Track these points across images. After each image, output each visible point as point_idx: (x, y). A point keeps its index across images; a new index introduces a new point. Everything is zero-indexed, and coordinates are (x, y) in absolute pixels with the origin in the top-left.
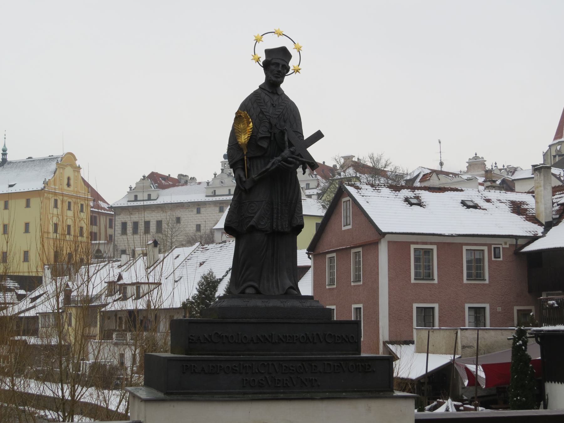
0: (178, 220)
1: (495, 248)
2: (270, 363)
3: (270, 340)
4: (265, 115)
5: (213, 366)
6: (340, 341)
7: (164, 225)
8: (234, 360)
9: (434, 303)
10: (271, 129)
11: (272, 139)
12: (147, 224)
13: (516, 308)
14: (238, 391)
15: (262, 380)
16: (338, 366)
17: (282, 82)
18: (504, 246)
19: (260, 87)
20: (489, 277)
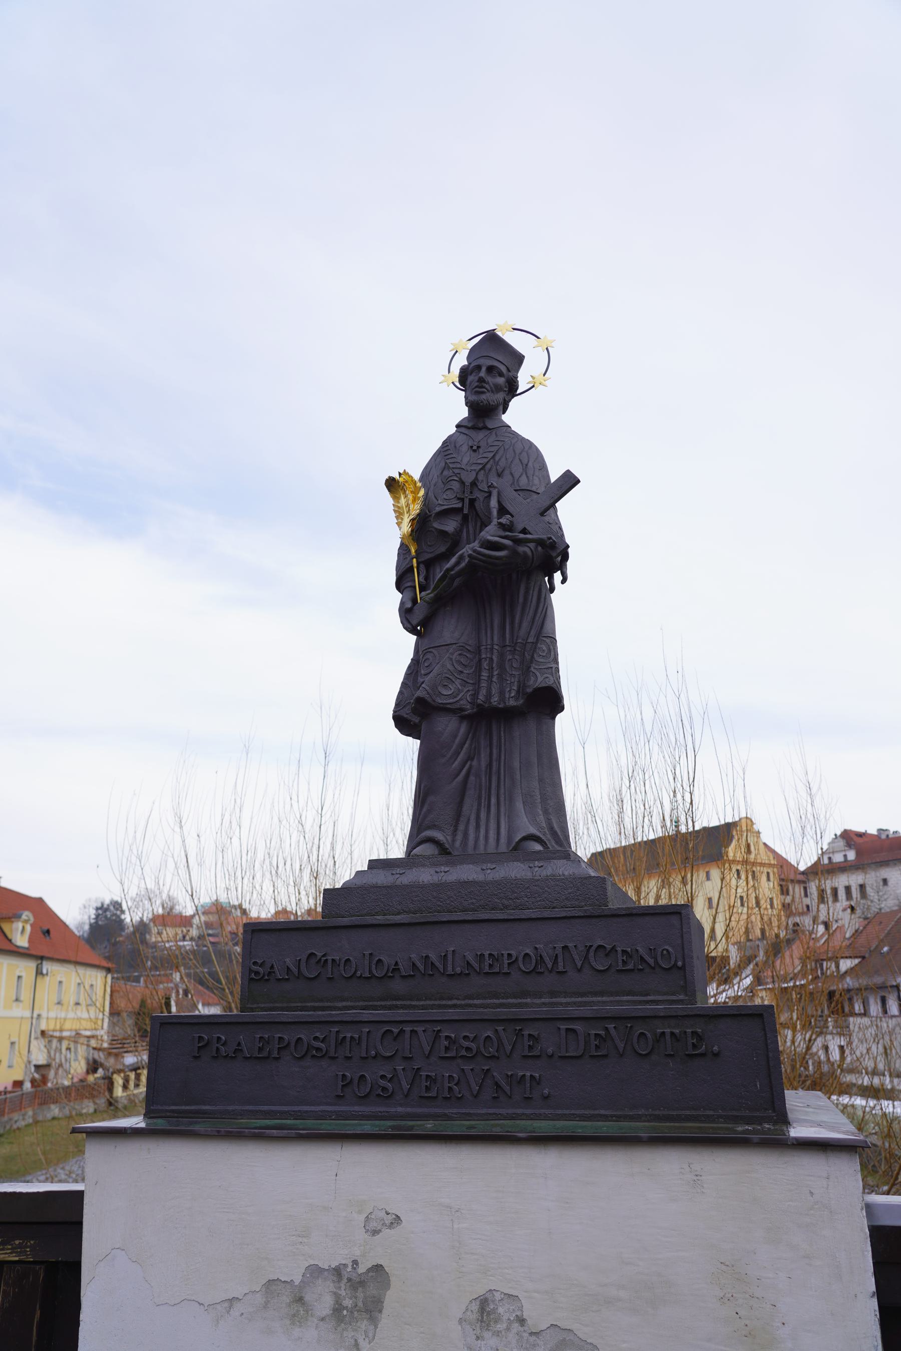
0: (885, 882)
6: (630, 967)
7: (868, 889)
8: (227, 1023)
12: (848, 889)
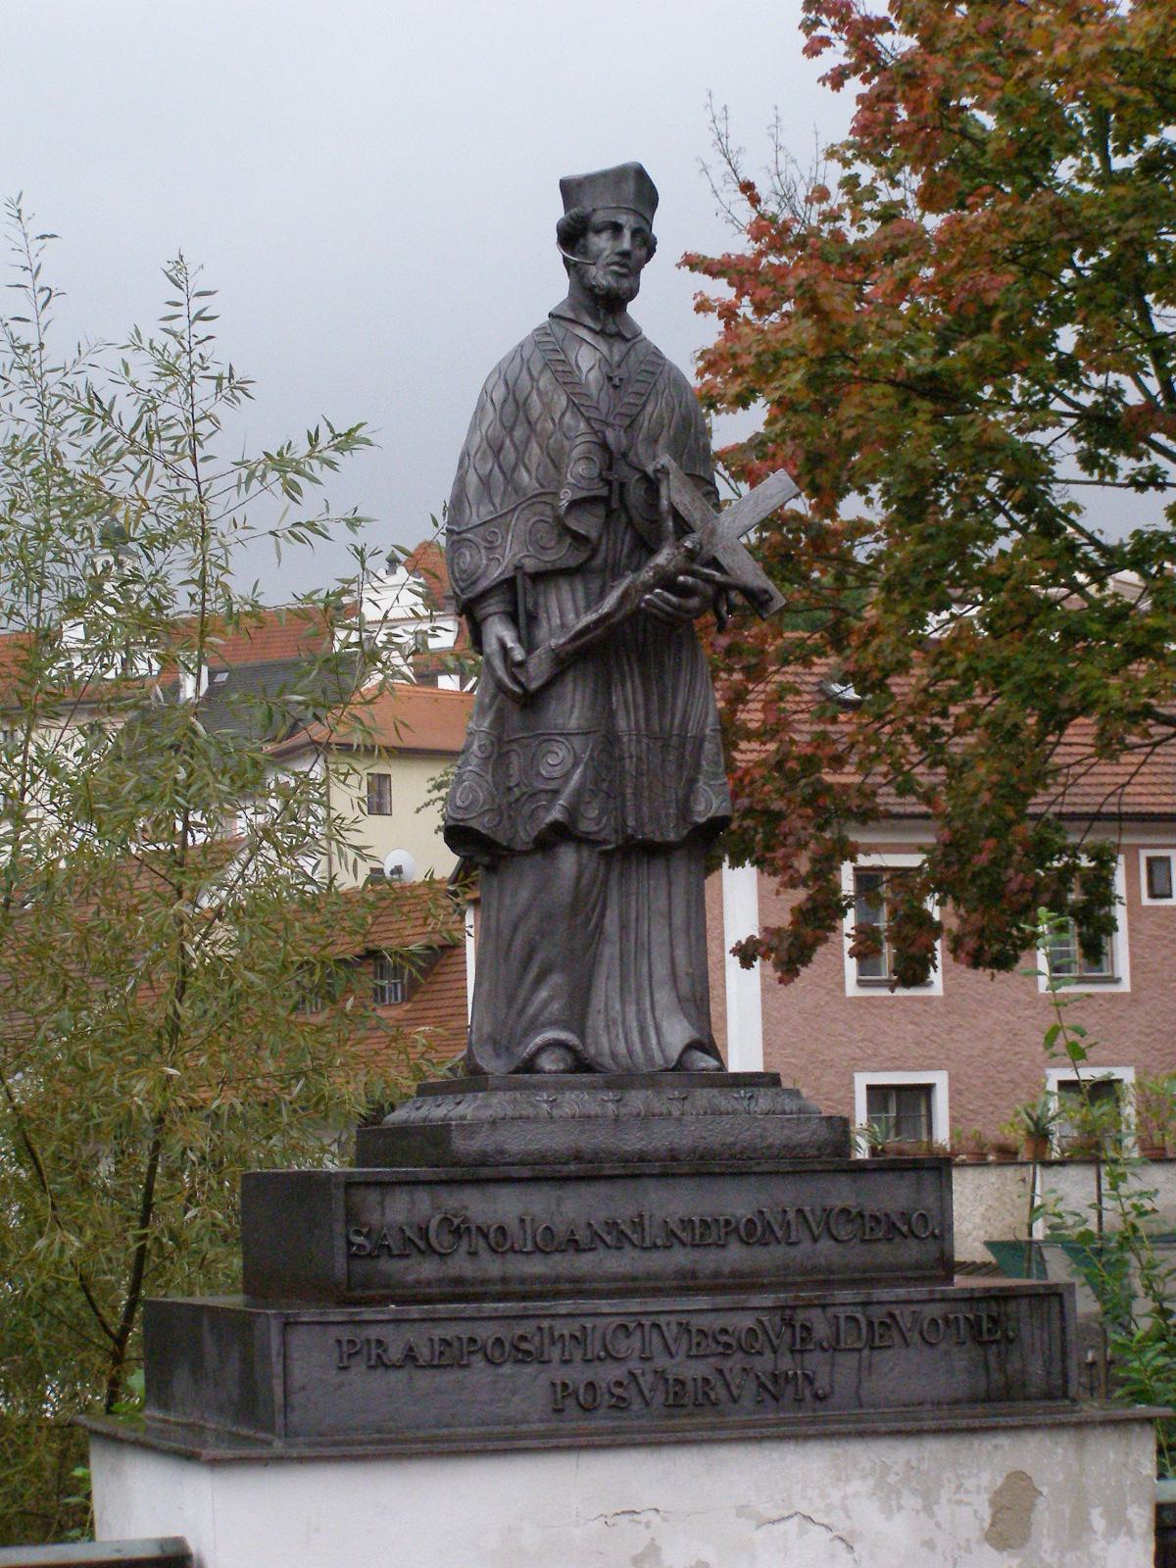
1: (1150, 861)
2: (646, 1321)
3: (635, 1237)
5: (444, 1341)
9: (930, 1068)
10: (610, 468)
11: (615, 504)
14: (574, 1425)
15: (619, 1384)
17: (632, 293)
20: (1134, 968)
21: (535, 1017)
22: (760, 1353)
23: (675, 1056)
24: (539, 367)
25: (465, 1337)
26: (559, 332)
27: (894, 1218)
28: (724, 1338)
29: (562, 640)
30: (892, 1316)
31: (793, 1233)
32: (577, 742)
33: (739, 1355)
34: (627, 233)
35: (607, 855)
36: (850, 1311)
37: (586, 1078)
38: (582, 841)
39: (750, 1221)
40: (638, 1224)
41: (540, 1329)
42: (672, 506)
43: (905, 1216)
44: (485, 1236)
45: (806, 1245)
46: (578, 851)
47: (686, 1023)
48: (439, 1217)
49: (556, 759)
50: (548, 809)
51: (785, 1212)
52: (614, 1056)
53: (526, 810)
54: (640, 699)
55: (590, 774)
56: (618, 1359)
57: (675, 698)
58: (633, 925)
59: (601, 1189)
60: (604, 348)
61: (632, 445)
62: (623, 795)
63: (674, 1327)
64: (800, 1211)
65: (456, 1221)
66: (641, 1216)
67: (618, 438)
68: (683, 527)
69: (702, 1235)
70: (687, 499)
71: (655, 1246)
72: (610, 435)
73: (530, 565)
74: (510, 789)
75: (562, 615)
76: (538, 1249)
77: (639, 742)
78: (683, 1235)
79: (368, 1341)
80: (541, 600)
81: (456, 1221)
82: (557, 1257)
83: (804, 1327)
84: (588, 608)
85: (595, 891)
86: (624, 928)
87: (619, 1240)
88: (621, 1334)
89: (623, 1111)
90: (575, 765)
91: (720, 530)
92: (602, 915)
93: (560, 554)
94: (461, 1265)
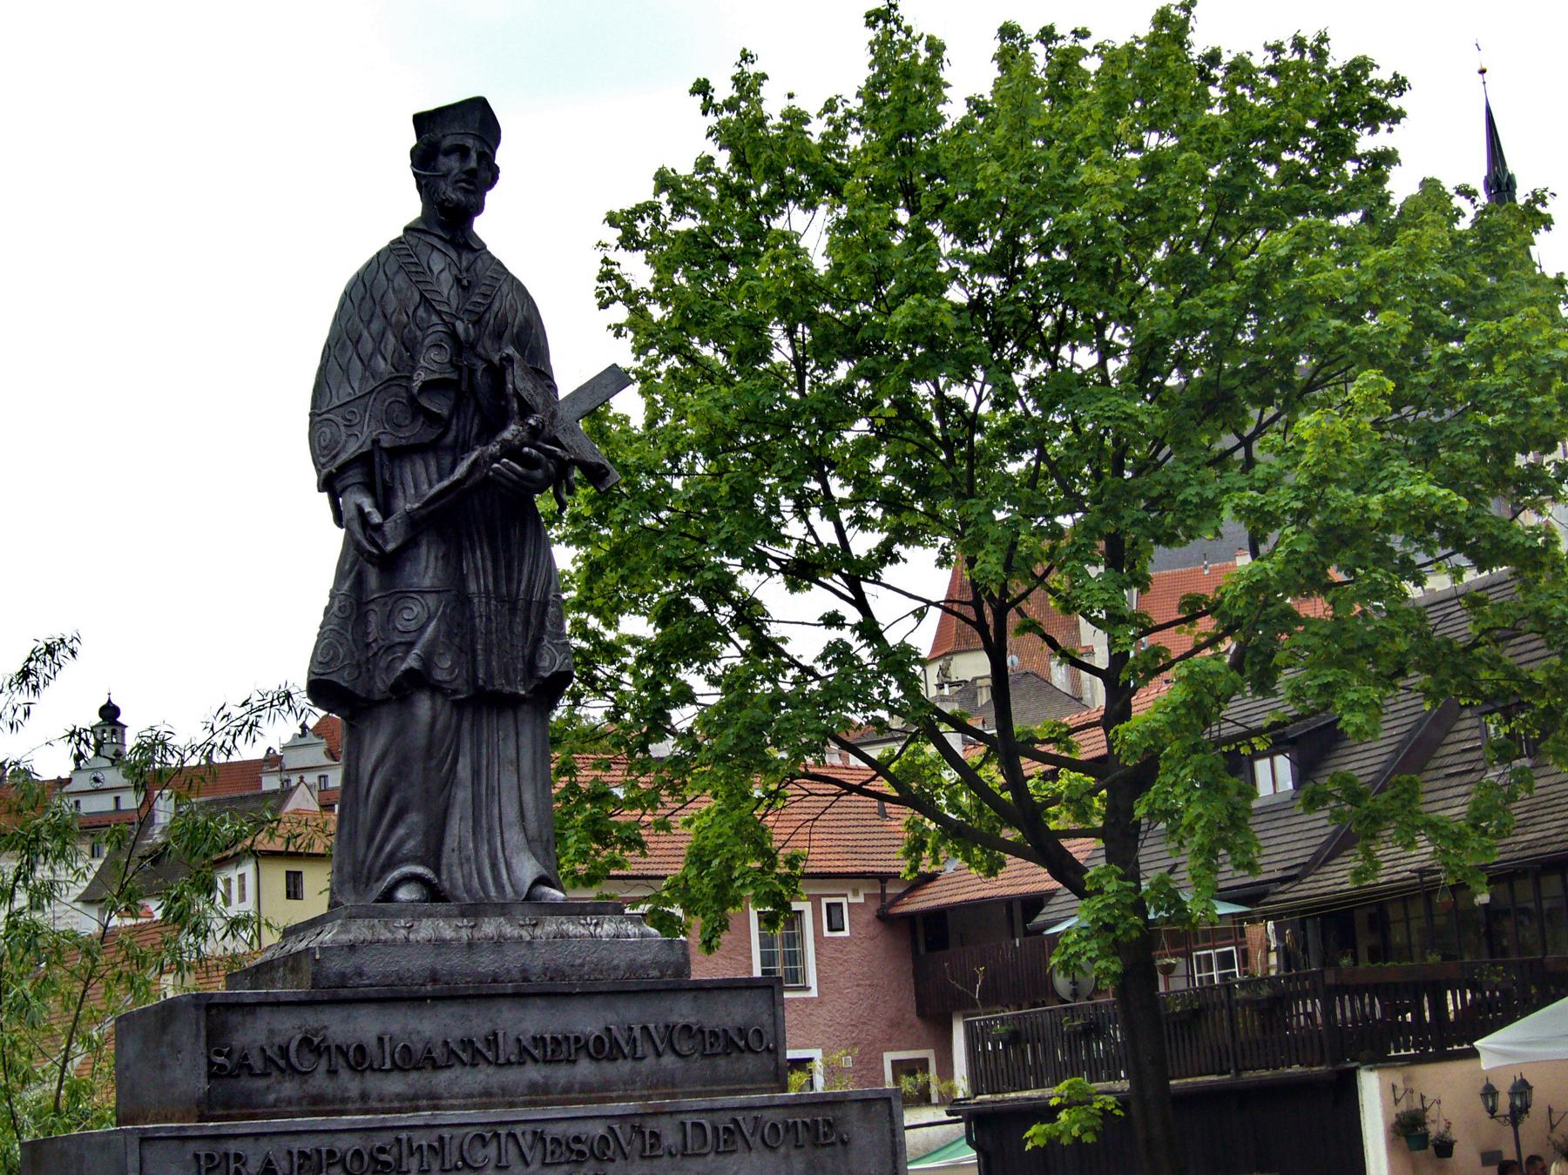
1: (828, 905)
2: (503, 1131)
3: (490, 1055)
4: (439, 313)
5: (302, 1154)
11: (464, 387)
13: (888, 1057)
16: (726, 1129)
17: (479, 209)
18: (852, 900)
19: (407, 229)
20: (819, 980)
21: (392, 854)
22: (612, 1160)
23: (526, 890)
24: (395, 268)
25: (324, 1149)
26: (413, 242)
27: (731, 1033)
28: (576, 1147)
29: (416, 505)
30: (735, 1121)
31: (639, 1049)
32: (431, 600)
33: (592, 1162)
34: (474, 155)
35: (459, 706)
36: (695, 1118)
37: (441, 907)
38: (436, 689)
39: (598, 1038)
40: (492, 1041)
41: (399, 1141)
42: (515, 389)
43: (741, 1032)
44: (345, 1055)
45: (651, 1060)
46: (432, 698)
47: (534, 861)
48: (299, 1037)
49: (412, 613)
50: (403, 659)
51: (631, 1029)
52: (469, 891)
53: (382, 664)
54: (489, 564)
55: (443, 628)
56: (475, 1169)
57: (521, 565)
58: (484, 771)
59: (457, 1009)
60: (454, 255)
61: (478, 338)
62: (474, 651)
63: (529, 1137)
64: (645, 1028)
65: (316, 1040)
66: (495, 1035)
67: (466, 329)
68: (526, 410)
69: (553, 1051)
70: (530, 386)
71: (509, 1063)
72: (460, 326)
73: (386, 442)
74: (368, 645)
75: (416, 487)
76: (396, 1067)
77: (488, 604)
78: (536, 1052)
79: (227, 1155)
80: (397, 473)
81: (316, 1040)
82: (414, 1075)
83: (653, 1134)
84: (441, 479)
85: (448, 740)
86: (476, 773)
87: (473, 1057)
88: (478, 1144)
89: (476, 935)
90: (429, 619)
91: (560, 414)
92: (455, 761)
93: (412, 432)
94: (319, 1082)
